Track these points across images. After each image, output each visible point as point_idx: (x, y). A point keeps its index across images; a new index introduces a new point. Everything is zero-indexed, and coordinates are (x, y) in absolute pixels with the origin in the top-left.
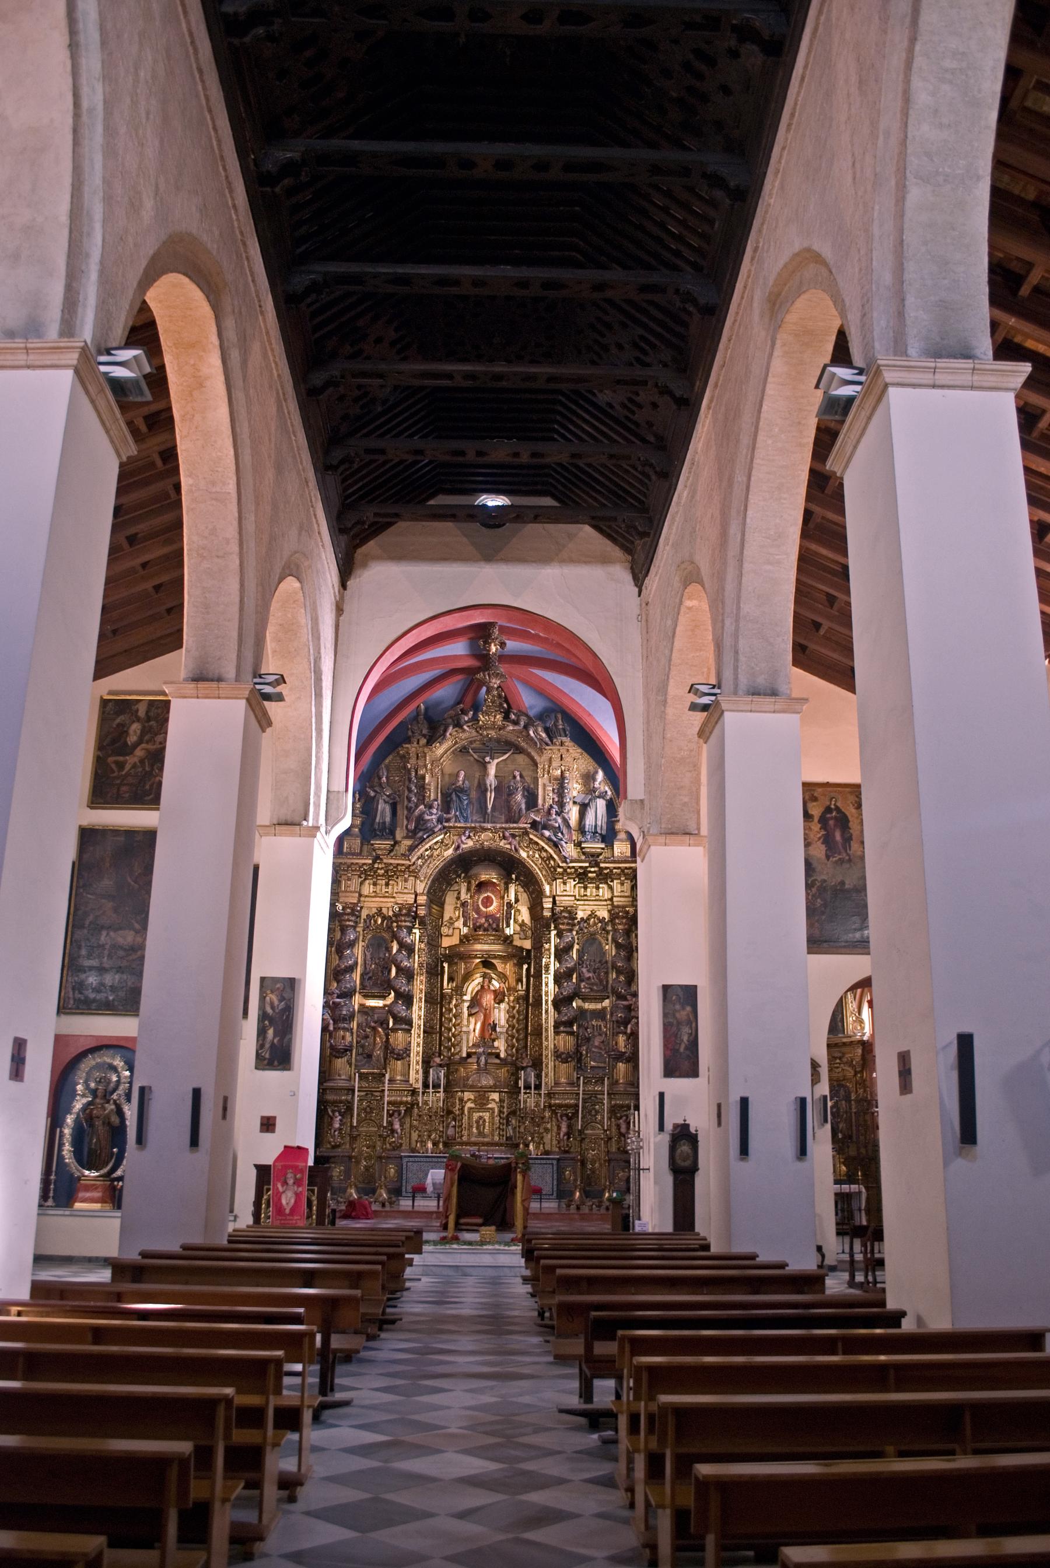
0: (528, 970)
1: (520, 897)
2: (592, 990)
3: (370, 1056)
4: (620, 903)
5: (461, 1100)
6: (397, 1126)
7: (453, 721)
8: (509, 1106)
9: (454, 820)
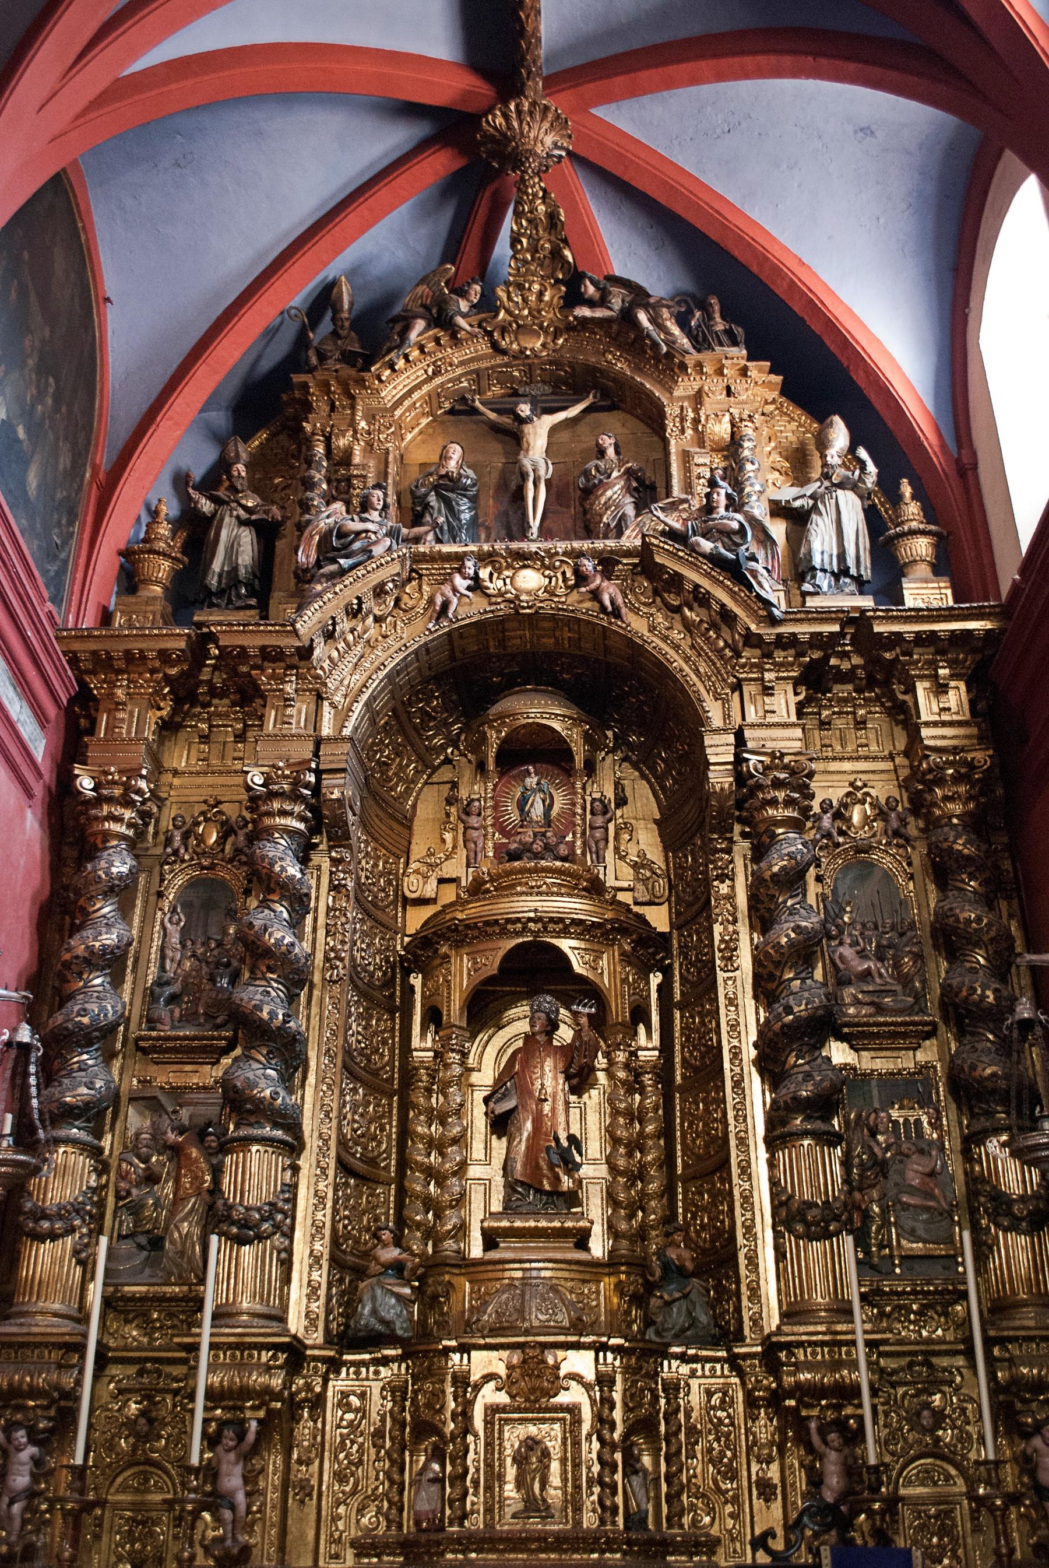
0: (664, 989)
1: (628, 793)
2: (880, 1009)
3: (156, 1243)
4: (940, 743)
5: (462, 1381)
6: (233, 1480)
8: (632, 1401)
9: (430, 537)
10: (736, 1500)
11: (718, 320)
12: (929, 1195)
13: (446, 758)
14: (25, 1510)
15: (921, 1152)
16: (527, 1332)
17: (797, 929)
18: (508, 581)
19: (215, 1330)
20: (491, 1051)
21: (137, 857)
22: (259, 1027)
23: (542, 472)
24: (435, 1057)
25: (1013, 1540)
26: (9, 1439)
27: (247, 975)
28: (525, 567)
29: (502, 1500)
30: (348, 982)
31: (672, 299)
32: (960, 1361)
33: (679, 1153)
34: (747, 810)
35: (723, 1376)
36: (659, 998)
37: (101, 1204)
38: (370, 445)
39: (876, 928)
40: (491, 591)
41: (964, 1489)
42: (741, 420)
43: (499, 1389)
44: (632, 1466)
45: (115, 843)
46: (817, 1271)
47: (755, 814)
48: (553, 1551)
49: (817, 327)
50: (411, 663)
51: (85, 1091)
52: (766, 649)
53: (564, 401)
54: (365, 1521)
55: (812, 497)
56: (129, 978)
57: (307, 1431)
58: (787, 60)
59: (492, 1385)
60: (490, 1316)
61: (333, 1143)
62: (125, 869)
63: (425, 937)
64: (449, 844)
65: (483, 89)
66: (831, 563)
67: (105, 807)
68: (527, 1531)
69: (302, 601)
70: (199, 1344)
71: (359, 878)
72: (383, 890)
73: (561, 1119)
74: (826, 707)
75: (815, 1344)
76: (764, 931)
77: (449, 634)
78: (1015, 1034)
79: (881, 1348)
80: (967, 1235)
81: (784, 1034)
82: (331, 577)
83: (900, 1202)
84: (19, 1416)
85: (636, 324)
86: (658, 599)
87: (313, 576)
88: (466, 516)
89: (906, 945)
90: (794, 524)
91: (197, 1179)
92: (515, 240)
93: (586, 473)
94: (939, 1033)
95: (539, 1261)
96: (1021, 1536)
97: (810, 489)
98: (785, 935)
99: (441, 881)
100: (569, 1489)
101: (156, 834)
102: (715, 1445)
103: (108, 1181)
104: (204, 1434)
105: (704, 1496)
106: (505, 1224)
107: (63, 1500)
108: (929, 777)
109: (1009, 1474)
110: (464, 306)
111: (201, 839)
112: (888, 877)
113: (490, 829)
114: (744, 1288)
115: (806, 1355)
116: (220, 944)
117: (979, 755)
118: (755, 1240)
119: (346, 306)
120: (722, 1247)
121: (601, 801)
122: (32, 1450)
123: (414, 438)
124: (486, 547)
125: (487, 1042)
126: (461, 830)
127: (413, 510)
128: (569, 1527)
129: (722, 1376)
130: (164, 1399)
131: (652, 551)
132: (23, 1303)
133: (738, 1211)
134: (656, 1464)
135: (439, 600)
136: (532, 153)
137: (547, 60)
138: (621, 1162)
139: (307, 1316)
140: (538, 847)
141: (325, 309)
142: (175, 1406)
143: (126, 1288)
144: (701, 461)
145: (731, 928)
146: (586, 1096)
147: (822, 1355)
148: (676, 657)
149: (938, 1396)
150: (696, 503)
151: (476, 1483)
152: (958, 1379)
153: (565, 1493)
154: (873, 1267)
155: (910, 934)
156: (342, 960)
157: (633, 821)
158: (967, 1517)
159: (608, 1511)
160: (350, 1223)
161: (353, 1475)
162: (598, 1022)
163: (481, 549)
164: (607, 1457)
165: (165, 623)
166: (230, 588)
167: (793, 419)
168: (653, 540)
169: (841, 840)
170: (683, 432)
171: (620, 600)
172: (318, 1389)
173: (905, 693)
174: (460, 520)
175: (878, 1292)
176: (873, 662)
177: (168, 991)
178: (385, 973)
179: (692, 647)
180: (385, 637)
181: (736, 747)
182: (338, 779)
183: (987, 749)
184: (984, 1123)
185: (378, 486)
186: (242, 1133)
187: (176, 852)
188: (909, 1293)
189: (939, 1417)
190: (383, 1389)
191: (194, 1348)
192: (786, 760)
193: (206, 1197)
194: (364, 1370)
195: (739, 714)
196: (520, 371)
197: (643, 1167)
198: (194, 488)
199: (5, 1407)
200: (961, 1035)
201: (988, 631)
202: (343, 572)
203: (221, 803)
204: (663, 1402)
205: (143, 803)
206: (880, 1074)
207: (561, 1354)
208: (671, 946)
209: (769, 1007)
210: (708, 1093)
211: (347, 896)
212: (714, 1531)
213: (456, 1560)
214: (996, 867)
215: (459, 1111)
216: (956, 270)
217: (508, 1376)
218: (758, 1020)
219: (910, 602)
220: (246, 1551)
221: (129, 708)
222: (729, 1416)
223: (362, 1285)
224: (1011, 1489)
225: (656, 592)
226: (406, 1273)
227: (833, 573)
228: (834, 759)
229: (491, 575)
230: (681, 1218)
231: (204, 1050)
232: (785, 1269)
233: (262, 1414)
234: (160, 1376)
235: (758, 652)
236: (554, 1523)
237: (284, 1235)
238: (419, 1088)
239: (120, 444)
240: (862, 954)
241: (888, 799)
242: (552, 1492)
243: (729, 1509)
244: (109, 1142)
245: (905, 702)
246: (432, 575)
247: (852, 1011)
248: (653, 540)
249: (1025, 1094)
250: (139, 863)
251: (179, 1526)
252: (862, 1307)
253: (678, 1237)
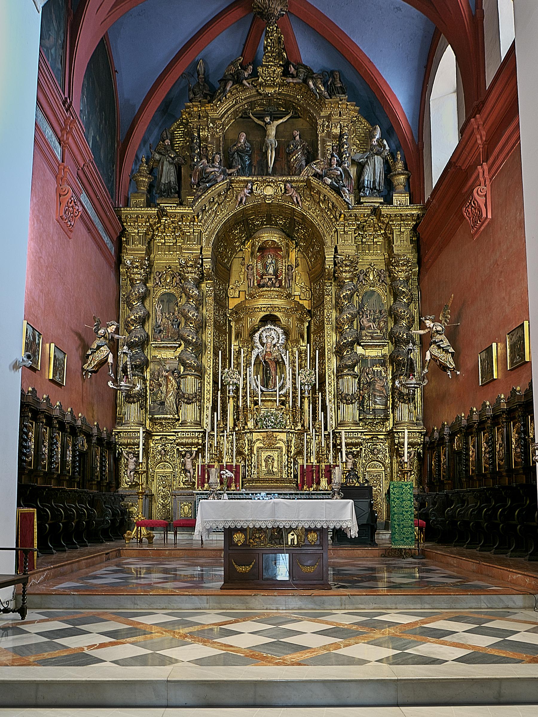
0: (309, 328)
7: (233, 76)
59: (259, 442)
116: (173, 314)
136: (273, 14)
159: (289, 474)
173: (390, 234)
186: (186, 372)
207: (277, 434)
216: (426, 67)
233: (196, 449)
245: (390, 237)
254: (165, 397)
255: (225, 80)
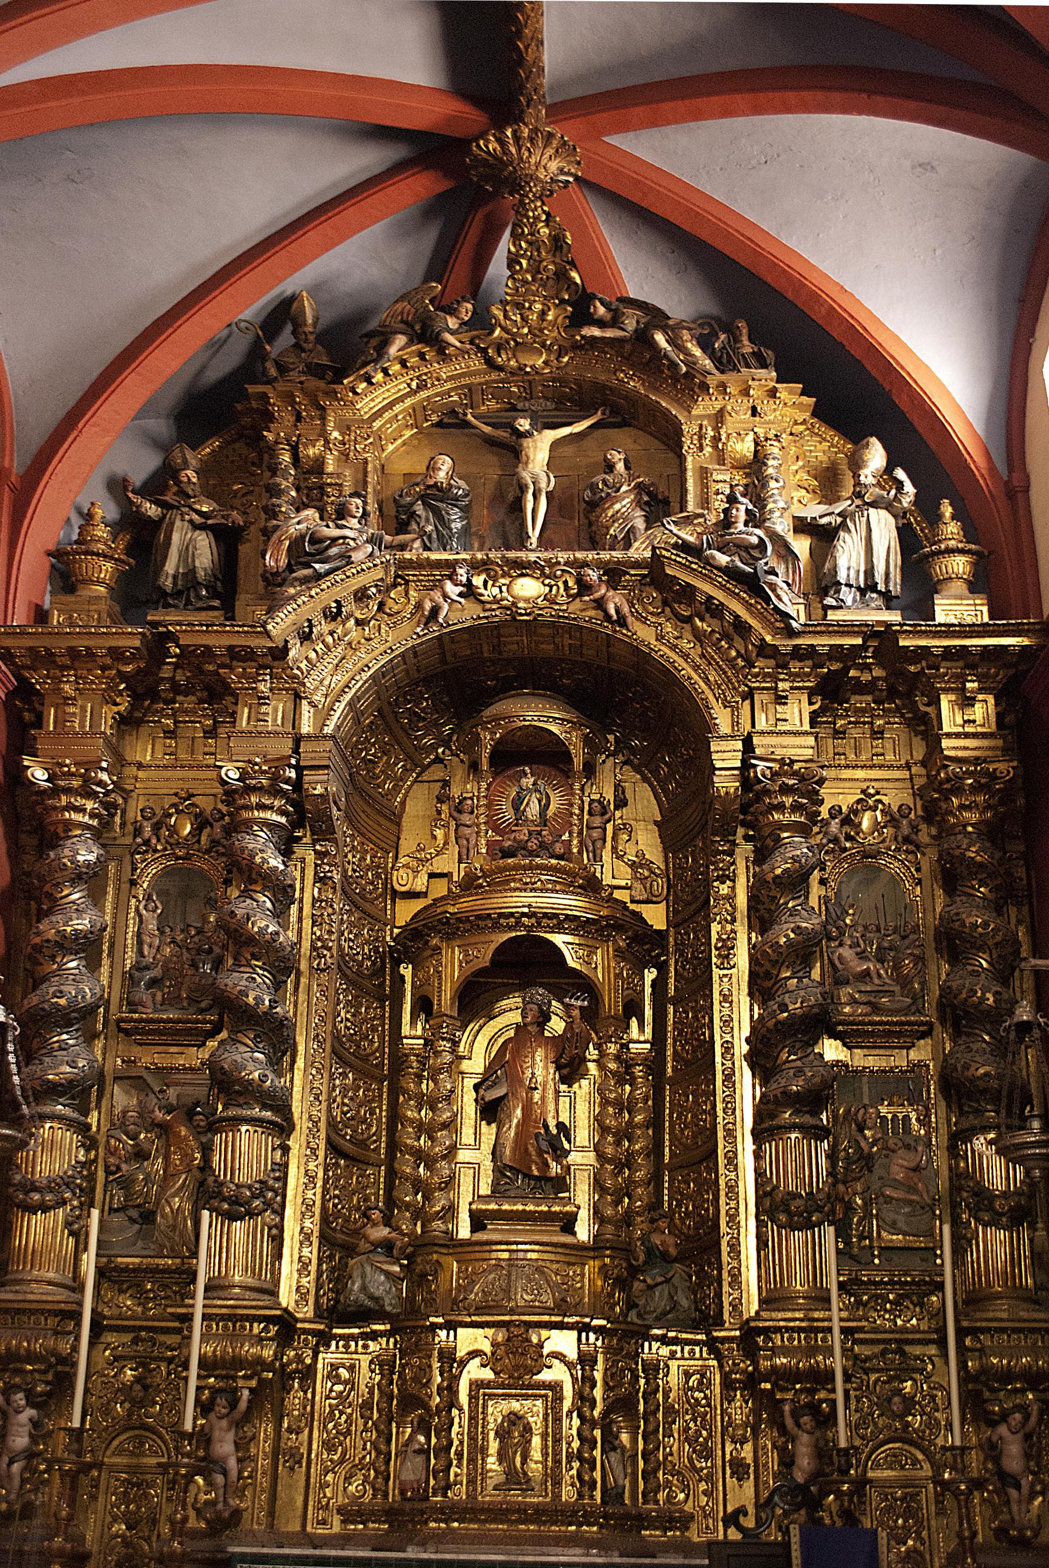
1: (629, 795)
2: (876, 1008)
3: (147, 1217)
4: (960, 754)
5: (448, 1356)
6: (225, 1446)
9: (417, 544)
10: (710, 1478)
11: (746, 342)
12: (912, 1189)
13: (437, 757)
14: (24, 1469)
15: (908, 1147)
16: (512, 1312)
17: (797, 930)
18: (504, 588)
19: (207, 1302)
20: (482, 1041)
21: (103, 846)
22: (245, 1011)
23: (543, 485)
24: (425, 1045)
25: (976, 1524)
26: (8, 1401)
27: (230, 962)
28: (523, 575)
29: (484, 1472)
30: (336, 970)
31: (694, 322)
32: (933, 1350)
33: (667, 1143)
34: (752, 814)
35: (701, 1358)
36: (653, 993)
37: (91, 1178)
38: (345, 455)
39: (878, 930)
40: (485, 598)
41: (930, 1474)
42: (767, 439)
43: (483, 1366)
44: (610, 1443)
45: (79, 832)
46: (798, 1260)
47: (761, 818)
48: (532, 1523)
49: (857, 352)
50: (398, 665)
51: (68, 1069)
52: (781, 660)
53: (569, 416)
54: (352, 1488)
55: (839, 515)
56: (106, 962)
57: (297, 1401)
58: (837, 97)
59: (477, 1361)
60: (476, 1294)
61: (322, 1125)
62: (92, 857)
63: (415, 929)
64: (440, 841)
65: (473, 116)
66: (857, 578)
67: (64, 798)
68: (507, 1503)
69: (274, 606)
70: (192, 1314)
71: (345, 871)
72: (372, 883)
73: (551, 1107)
74: (841, 717)
75: (792, 1329)
76: (762, 932)
77: (439, 638)
78: (1012, 1036)
79: (856, 1336)
80: (947, 1229)
81: (778, 1030)
82: (305, 581)
83: (883, 1195)
84: (17, 1379)
85: (653, 345)
86: (668, 609)
87: (284, 580)
88: (457, 526)
89: (907, 948)
90: (820, 540)
91: (187, 1157)
92: (512, 261)
93: (593, 487)
94: (934, 1033)
95: (525, 1243)
96: (983, 1521)
97: (838, 508)
98: (784, 934)
99: (432, 875)
100: (550, 1464)
101: (123, 825)
102: (692, 1425)
103: (96, 1156)
104: (197, 1401)
105: (679, 1473)
106: (493, 1206)
107: (61, 1461)
108: (947, 786)
109: (974, 1460)
110: (452, 323)
111: (174, 830)
112: (895, 881)
113: (483, 827)
114: (725, 1274)
115: (782, 1341)
117: (1002, 766)
118: (738, 1228)
119: (310, 321)
120: (705, 1234)
121: (599, 802)
122: (31, 1412)
123: (397, 449)
124: (479, 556)
125: (478, 1032)
126: (453, 827)
127: (397, 517)
128: (548, 1500)
129: (699, 1359)
130: (159, 1367)
131: (663, 563)
132: (17, 1271)
133: (723, 1199)
134: (634, 1441)
135: (428, 605)
137: (551, 88)
138: (609, 1150)
139: (298, 1290)
140: (533, 845)
141: (284, 323)
142: (169, 1374)
143: (119, 1259)
144: (720, 477)
145: (729, 927)
146: (576, 1085)
147: (799, 1340)
148: (685, 665)
149: (909, 1383)
150: (712, 518)
151: (459, 1455)
152: (930, 1367)
153: (545, 1467)
154: (852, 1257)
155: (912, 937)
156: (329, 949)
157: (632, 822)
158: (932, 1500)
159: (586, 1485)
160: (340, 1202)
161: (341, 1444)
162: (591, 1015)
163: (473, 558)
164: (586, 1433)
165: (113, 621)
166: (188, 589)
167: (825, 440)
168: (664, 552)
169: (848, 845)
170: (701, 449)
171: (626, 609)
172: (308, 1361)
173: (928, 705)
174: (451, 529)
175: (857, 1281)
176: (896, 674)
177: (148, 975)
178: (374, 963)
179: (702, 656)
180: (369, 640)
181: (743, 753)
182: (321, 775)
183: (1012, 761)
184: (972, 1120)
185: (356, 494)
187: (147, 843)
188: (886, 1283)
189: (909, 1403)
190: (371, 1362)
191: (188, 1318)
192: (796, 767)
193: (197, 1173)
194: (353, 1344)
195: (749, 721)
196: (518, 387)
197: (630, 1155)
198: (133, 492)
199: (4, 1370)
200: (956, 1035)
201: (1024, 647)
202: (319, 577)
203: (194, 796)
204: (642, 1381)
205: (106, 794)
206: (872, 1071)
207: (544, 1333)
208: (668, 942)
209: (763, 1004)
210: (699, 1085)
211: (334, 888)
212: (688, 1507)
213: (439, 1528)
214: (1009, 874)
215: (449, 1097)
216: (1022, 301)
217: (493, 1354)
218: (752, 1016)
219: (940, 617)
220: (237, 1514)
221: (80, 702)
222: (706, 1397)
223: (351, 1262)
224: (975, 1475)
225: (665, 603)
226: (395, 1252)
227: (859, 588)
228: (847, 767)
229: (485, 583)
230: (666, 1205)
231: (188, 1032)
232: (767, 1256)
234: (154, 1345)
235: (772, 662)
236: (534, 1496)
237: (274, 1212)
238: (410, 1074)
239: (34, 448)
240: (862, 956)
241: (900, 807)
242: (533, 1466)
243: (703, 1486)
244: (95, 1119)
245: (927, 713)
246: (420, 581)
247: (847, 1010)
248: (664, 552)
249: (1017, 1094)
250: (107, 852)
251: (173, 1489)
252: (840, 1296)
253: (662, 1224)
254: (159, 1196)
255: (383, 333)
